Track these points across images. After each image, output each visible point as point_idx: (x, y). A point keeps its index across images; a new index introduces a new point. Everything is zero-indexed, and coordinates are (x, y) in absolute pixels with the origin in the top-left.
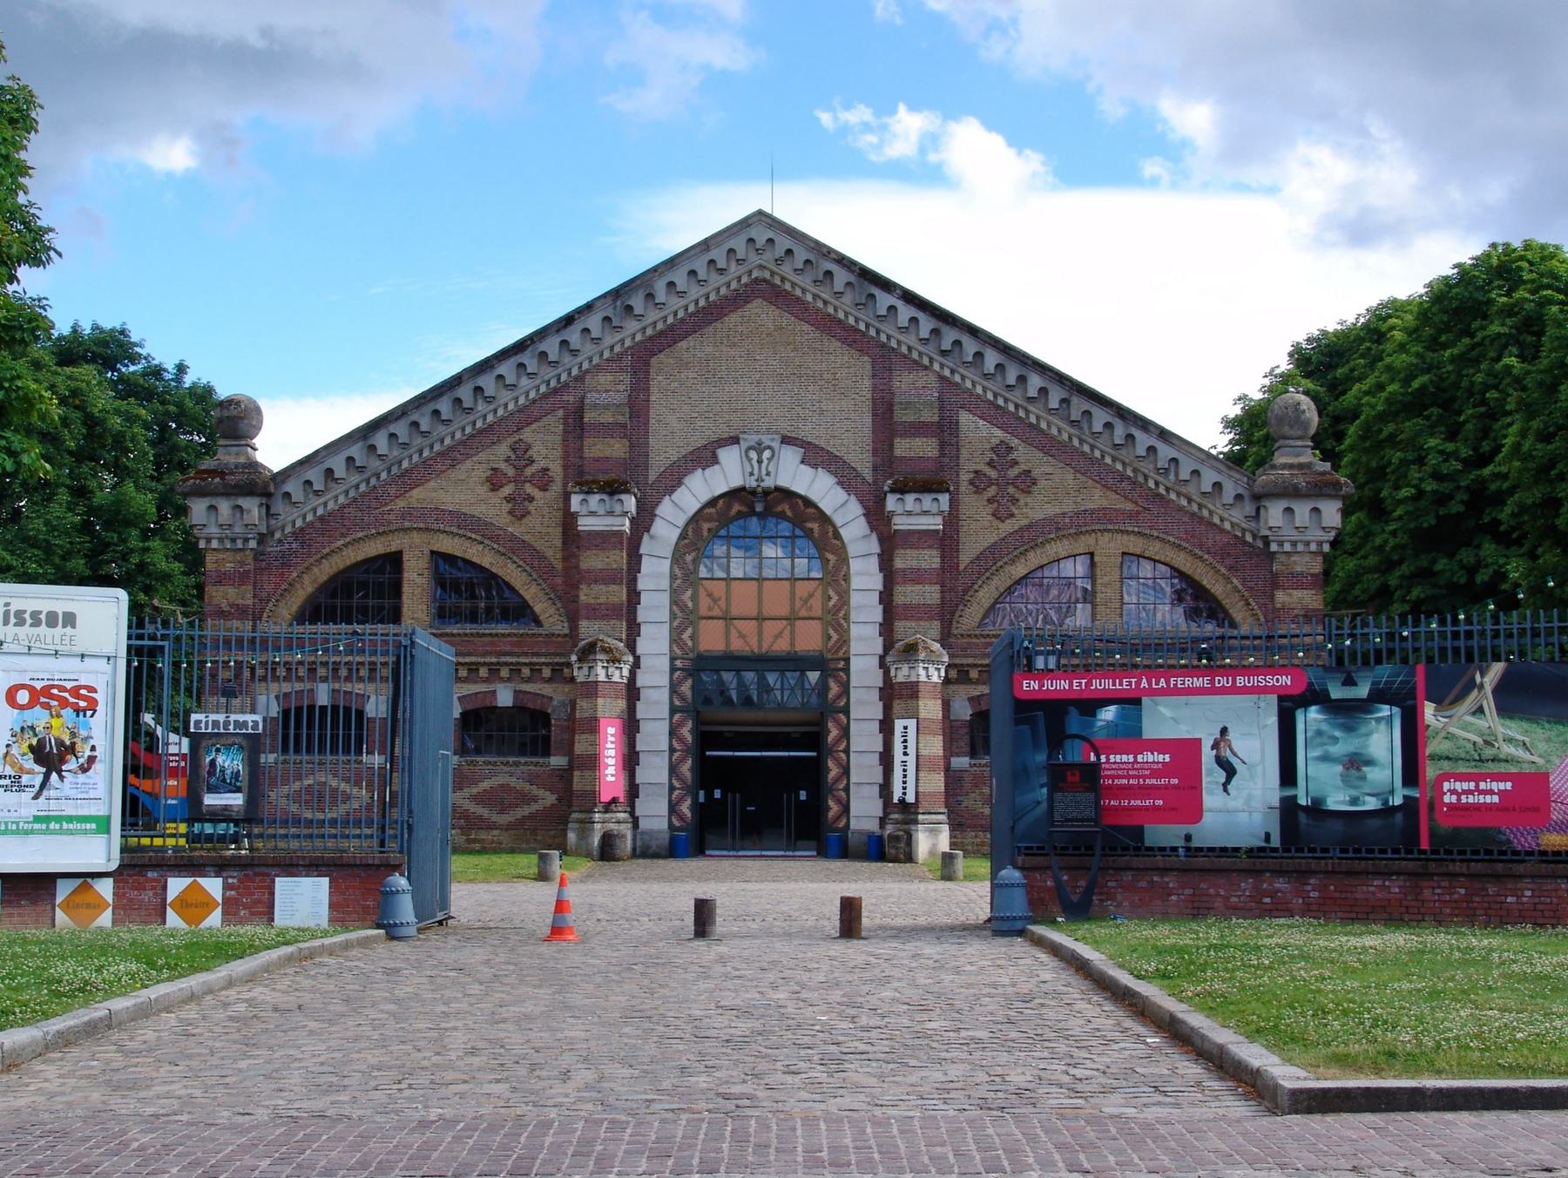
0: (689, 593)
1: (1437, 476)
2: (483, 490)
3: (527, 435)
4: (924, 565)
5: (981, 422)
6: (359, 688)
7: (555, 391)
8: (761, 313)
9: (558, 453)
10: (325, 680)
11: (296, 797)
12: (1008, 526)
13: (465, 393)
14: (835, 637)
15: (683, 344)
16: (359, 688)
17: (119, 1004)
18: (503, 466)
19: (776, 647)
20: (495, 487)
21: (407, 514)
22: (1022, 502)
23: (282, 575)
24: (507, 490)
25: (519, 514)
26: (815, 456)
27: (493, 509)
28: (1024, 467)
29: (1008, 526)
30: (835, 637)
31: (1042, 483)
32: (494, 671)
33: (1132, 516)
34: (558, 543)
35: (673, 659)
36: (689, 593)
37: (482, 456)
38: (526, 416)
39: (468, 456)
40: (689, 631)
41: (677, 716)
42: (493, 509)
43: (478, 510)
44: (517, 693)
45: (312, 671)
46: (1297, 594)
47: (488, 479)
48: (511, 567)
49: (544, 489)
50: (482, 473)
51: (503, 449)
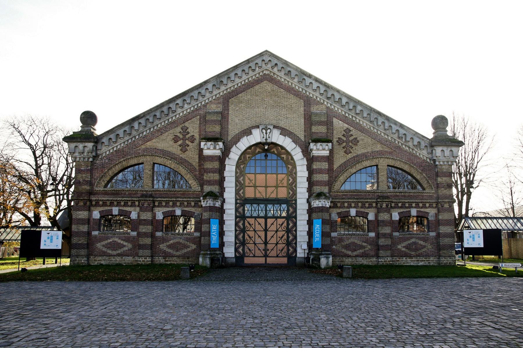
0: (242, 178)
2: (172, 143)
3: (187, 124)
4: (323, 168)
5: (340, 122)
7: (197, 110)
8: (267, 86)
9: (197, 130)
12: (350, 156)
19: (271, 196)
20: (176, 142)
21: (146, 149)
22: (354, 148)
24: (180, 142)
25: (184, 150)
27: (175, 149)
28: (354, 137)
29: (350, 156)
30: (291, 193)
31: (361, 142)
33: (390, 153)
34: (197, 160)
35: (236, 200)
36: (242, 178)
40: (242, 191)
41: (238, 219)
43: (170, 149)
46: (444, 179)
47: (173, 139)
50: (171, 137)
51: (179, 129)
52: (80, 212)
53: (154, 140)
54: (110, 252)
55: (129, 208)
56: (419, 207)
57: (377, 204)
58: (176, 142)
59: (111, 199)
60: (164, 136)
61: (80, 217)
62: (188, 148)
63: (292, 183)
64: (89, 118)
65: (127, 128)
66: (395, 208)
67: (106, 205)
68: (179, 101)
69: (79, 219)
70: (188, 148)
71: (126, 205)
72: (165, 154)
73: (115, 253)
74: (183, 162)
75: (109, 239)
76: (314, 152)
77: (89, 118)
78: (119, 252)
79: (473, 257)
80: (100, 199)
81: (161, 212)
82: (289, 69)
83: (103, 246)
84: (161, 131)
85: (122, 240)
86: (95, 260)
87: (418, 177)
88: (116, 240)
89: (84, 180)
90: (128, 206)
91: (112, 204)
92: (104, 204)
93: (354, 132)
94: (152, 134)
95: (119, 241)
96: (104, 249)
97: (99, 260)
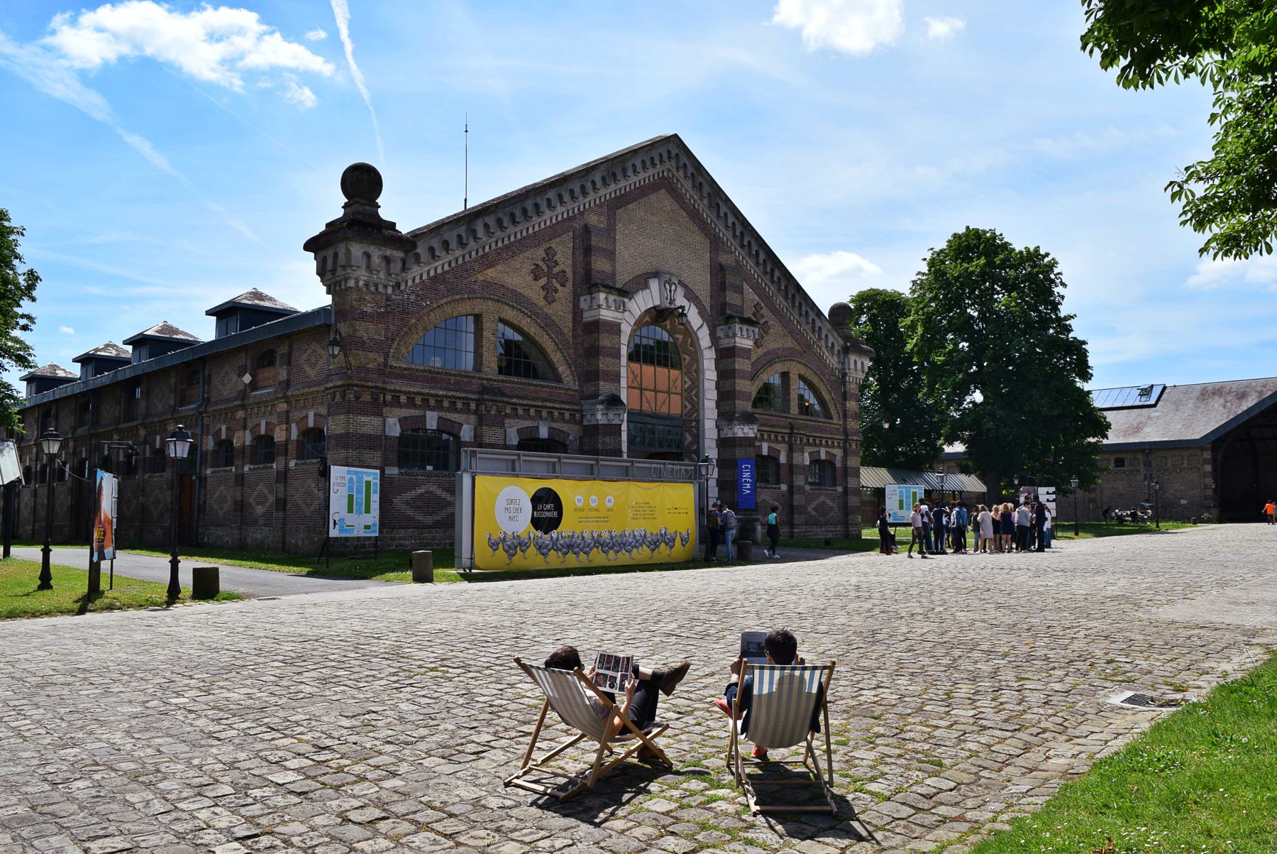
1: (367, 285)
2: (530, 278)
3: (553, 244)
6: (455, 417)
7: (569, 218)
9: (570, 262)
10: (433, 409)
11: (412, 504)
13: (529, 205)
14: (689, 406)
15: (630, 206)
16: (455, 417)
17: (96, 290)
18: (541, 263)
20: (536, 278)
21: (487, 285)
23: (403, 319)
24: (543, 281)
25: (549, 300)
26: (691, 296)
27: (534, 292)
30: (689, 406)
32: (539, 410)
34: (570, 325)
37: (528, 254)
38: (554, 231)
39: (522, 251)
42: (534, 292)
43: (527, 292)
44: (550, 428)
45: (426, 401)
47: (533, 271)
48: (546, 337)
49: (563, 285)
50: (528, 267)
51: (541, 253)
52: (363, 419)
53: (500, 267)
54: (421, 518)
55: (456, 415)
56: (553, 420)
57: (477, 406)
58: (536, 278)
59: (426, 391)
60: (516, 263)
61: (364, 430)
62: (557, 296)
63: (690, 390)
64: (362, 183)
65: (462, 230)
66: (391, 405)
67: (414, 406)
68: (551, 194)
69: (363, 436)
70: (557, 296)
71: (452, 408)
72: (518, 300)
73: (429, 520)
74: (548, 324)
75: (419, 486)
76: (586, 315)
77: (362, 183)
78: (439, 518)
79: (547, 509)
80: (403, 389)
81: (515, 429)
82: (701, 179)
83: (407, 503)
84: (512, 250)
85: (444, 490)
86: (393, 539)
87: (827, 397)
88: (433, 488)
89: (372, 340)
90: (456, 411)
91: (426, 405)
92: (411, 403)
93: (765, 311)
94: (499, 252)
95: (439, 492)
96: (410, 512)
97: (400, 538)
